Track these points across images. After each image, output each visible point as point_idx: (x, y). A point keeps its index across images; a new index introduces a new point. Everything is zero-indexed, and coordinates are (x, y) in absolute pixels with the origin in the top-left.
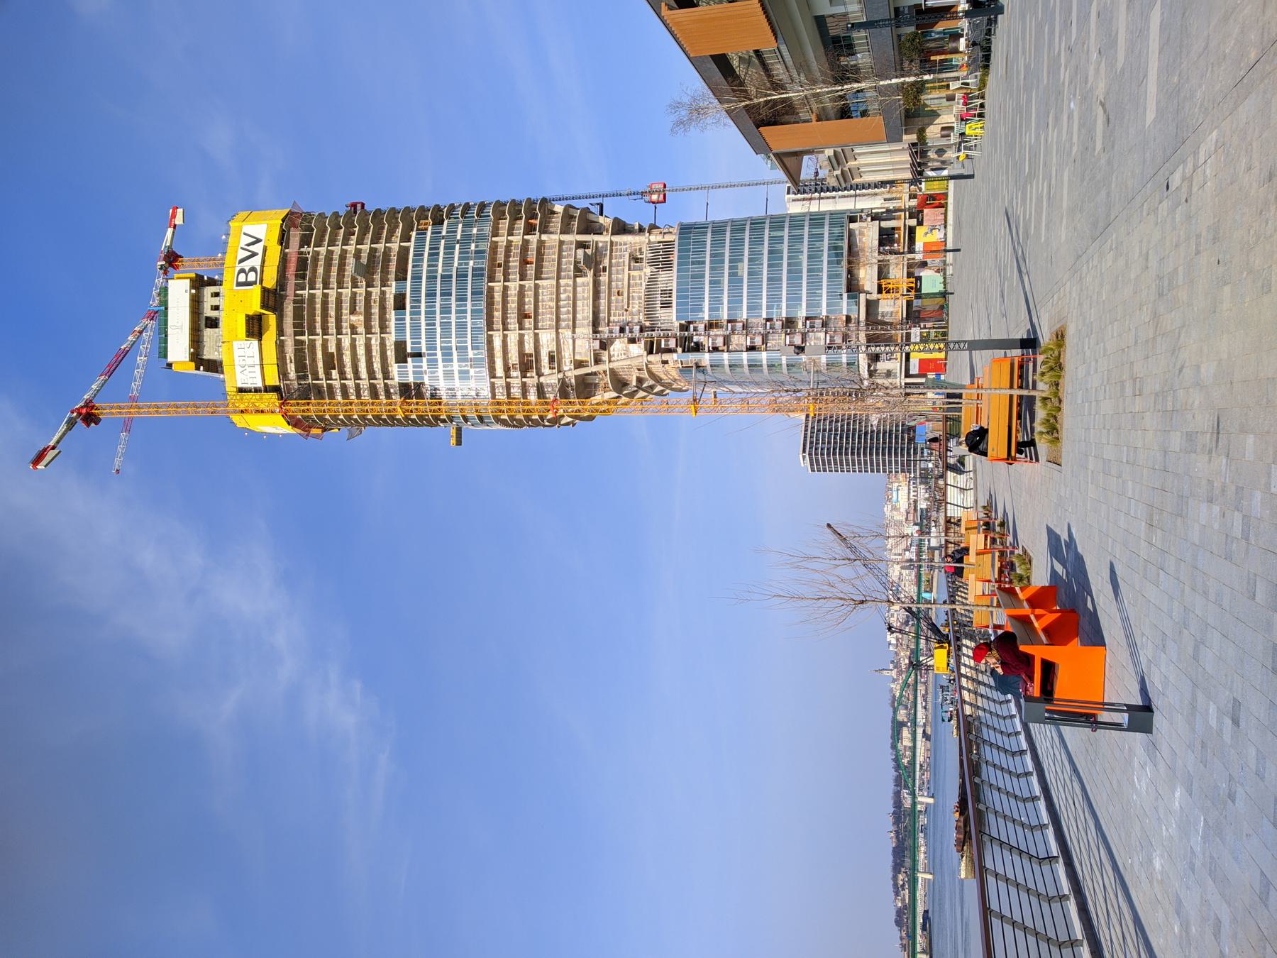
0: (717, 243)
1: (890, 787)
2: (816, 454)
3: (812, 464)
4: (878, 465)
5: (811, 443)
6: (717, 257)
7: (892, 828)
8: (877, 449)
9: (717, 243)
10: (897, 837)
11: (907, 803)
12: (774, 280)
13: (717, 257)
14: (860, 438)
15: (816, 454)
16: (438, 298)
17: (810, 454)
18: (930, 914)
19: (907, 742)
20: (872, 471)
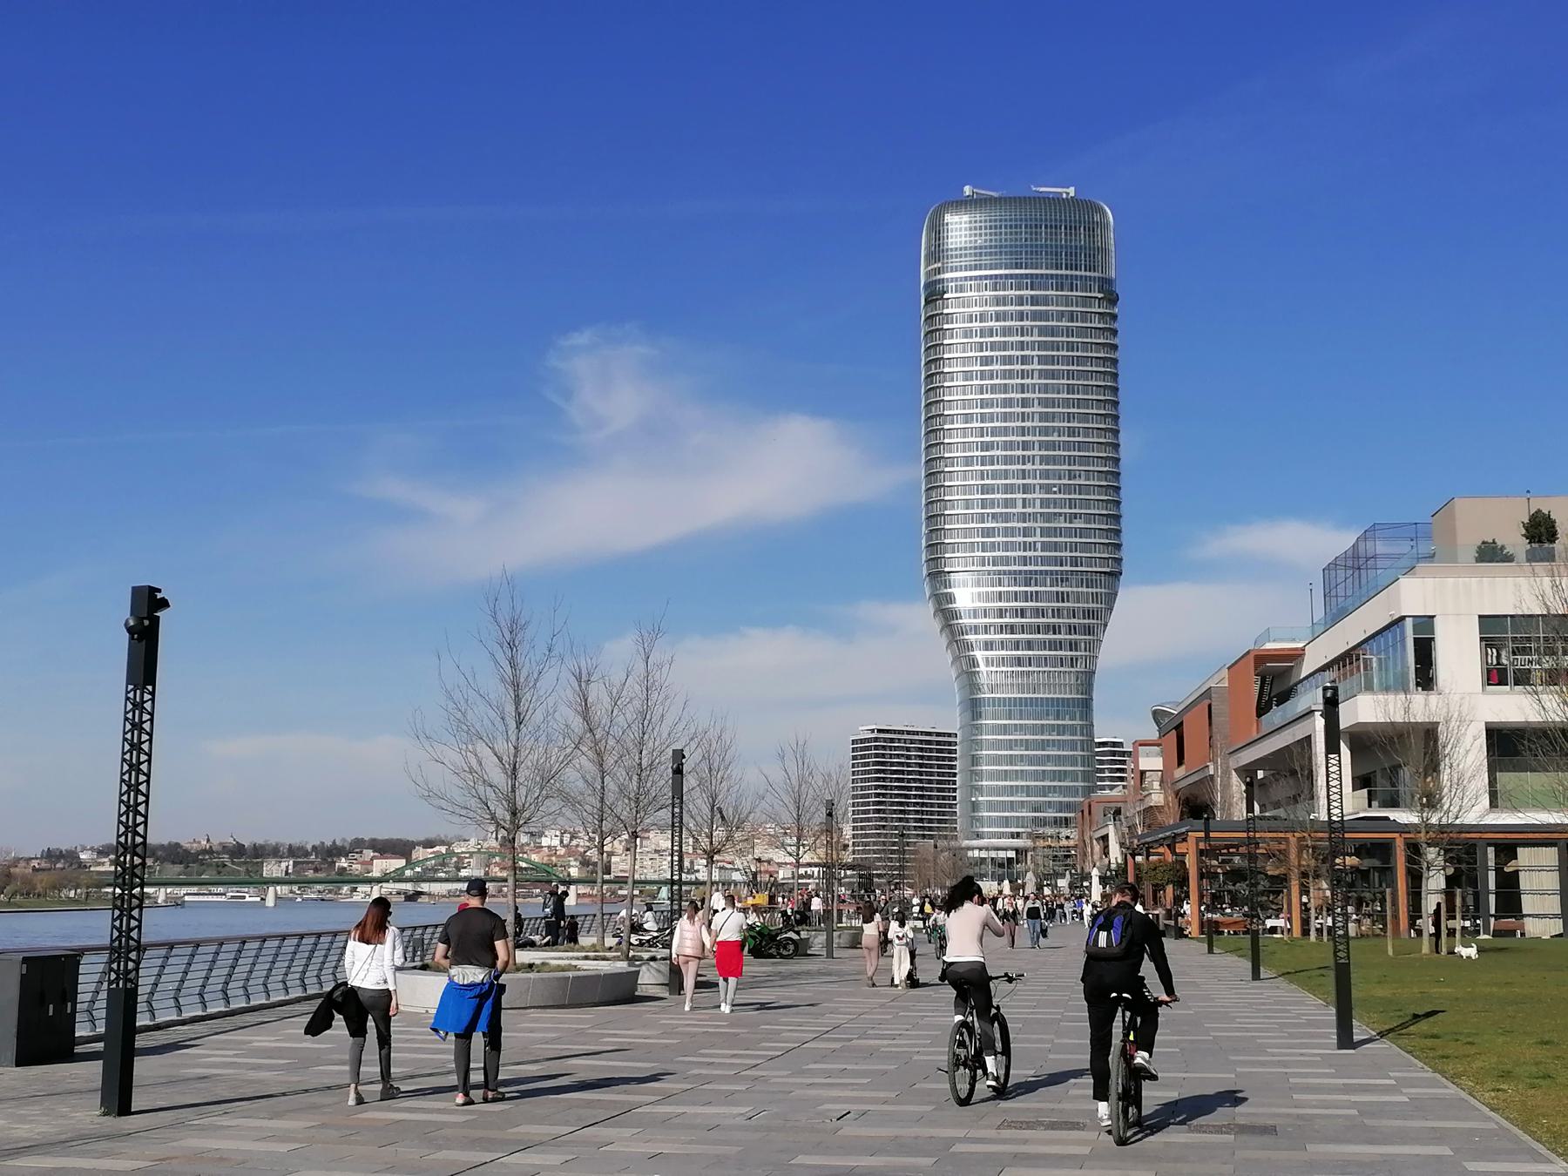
0: (1072, 730)
1: (287, 838)
2: (876, 748)
3: (862, 741)
4: (863, 757)
5: (892, 740)
6: (1061, 730)
7: (215, 842)
8: (884, 795)
9: (1072, 730)
10: (204, 852)
11: (272, 869)
12: (1043, 775)
13: (1061, 730)
14: (901, 804)
15: (876, 748)
16: (1020, 396)
17: (876, 739)
18: (1222, 1114)
19: (380, 866)
20: (854, 758)
